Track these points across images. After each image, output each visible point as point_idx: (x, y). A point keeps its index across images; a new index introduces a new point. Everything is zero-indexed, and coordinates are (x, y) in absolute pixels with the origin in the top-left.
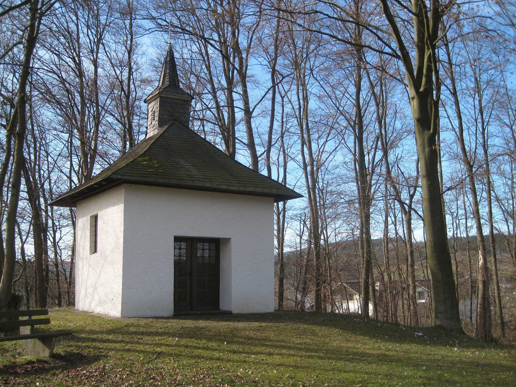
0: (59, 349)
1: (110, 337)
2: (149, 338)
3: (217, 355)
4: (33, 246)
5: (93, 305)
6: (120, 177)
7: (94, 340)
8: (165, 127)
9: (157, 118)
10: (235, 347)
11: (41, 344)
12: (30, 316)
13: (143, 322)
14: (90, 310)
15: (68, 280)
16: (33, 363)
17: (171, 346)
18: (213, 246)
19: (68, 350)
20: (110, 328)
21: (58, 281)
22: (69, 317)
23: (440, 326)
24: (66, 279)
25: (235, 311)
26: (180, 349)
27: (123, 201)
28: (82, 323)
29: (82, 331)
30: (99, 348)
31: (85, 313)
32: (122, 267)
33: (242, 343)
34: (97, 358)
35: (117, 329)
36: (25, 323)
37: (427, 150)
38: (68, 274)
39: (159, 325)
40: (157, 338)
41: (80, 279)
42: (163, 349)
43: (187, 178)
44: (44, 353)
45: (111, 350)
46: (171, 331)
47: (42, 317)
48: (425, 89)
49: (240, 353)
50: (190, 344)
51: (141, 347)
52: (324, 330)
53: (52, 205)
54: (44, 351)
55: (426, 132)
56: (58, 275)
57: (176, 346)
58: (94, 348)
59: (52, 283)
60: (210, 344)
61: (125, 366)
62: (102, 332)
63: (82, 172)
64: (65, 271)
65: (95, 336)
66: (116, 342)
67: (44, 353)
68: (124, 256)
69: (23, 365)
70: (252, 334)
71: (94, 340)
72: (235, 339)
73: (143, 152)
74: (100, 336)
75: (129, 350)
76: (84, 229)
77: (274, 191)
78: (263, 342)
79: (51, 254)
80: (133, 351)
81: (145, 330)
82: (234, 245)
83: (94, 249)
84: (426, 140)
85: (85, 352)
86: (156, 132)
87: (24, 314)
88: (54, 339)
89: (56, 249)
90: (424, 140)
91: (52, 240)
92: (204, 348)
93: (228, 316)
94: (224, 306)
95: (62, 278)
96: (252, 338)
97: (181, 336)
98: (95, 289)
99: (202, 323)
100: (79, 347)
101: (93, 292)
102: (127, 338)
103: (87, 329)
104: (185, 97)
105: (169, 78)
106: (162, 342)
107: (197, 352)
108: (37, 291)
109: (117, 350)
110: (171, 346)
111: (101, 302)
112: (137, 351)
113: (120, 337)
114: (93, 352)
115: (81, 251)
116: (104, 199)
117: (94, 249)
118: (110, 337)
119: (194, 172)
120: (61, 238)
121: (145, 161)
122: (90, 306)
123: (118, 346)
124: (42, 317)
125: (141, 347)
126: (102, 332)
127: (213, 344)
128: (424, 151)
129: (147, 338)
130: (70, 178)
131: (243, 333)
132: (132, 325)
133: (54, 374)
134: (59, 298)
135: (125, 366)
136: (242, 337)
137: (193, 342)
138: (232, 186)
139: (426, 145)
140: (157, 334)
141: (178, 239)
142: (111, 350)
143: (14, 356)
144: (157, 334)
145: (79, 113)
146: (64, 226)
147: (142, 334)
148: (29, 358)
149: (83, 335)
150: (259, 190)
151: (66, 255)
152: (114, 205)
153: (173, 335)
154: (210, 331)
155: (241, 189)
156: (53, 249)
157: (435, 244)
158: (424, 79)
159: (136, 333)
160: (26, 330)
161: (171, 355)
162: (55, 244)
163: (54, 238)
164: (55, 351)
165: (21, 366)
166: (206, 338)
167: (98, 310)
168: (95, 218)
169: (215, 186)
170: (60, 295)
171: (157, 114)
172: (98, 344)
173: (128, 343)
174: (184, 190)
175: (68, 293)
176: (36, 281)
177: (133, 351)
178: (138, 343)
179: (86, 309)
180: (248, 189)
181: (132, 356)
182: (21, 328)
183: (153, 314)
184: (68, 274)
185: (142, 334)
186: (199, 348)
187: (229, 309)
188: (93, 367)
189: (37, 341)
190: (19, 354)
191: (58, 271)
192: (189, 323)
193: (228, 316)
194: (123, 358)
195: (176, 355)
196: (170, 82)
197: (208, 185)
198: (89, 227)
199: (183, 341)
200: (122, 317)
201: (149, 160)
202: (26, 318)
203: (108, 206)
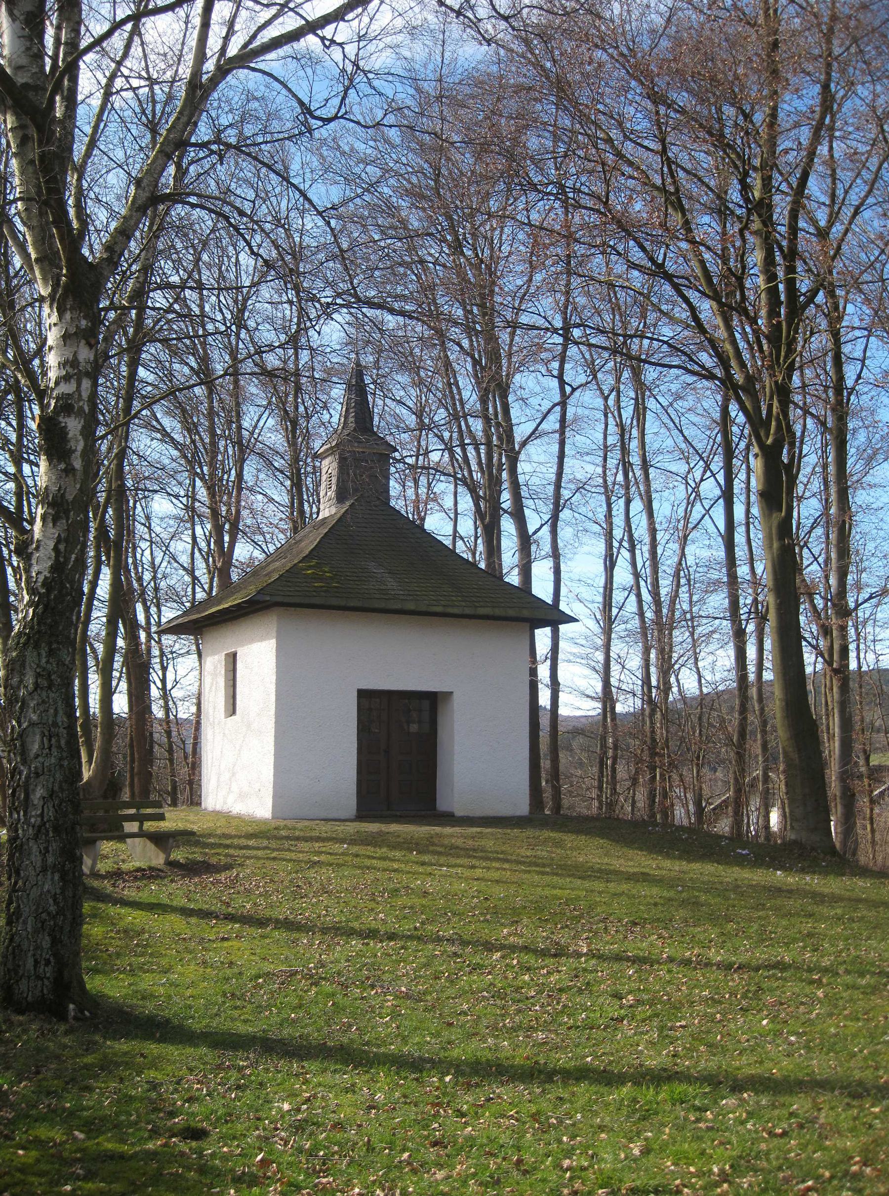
0: (179, 855)
1: (251, 843)
2: (306, 844)
3: (396, 866)
4: (126, 697)
5: (230, 800)
6: (268, 598)
7: (227, 847)
8: (348, 504)
9: (334, 487)
10: (426, 858)
11: (153, 846)
12: (138, 809)
13: (300, 825)
14: (225, 809)
15: (190, 760)
16: (144, 870)
17: (336, 854)
18: (426, 704)
19: (190, 857)
20: (252, 831)
21: (171, 760)
22: (192, 818)
23: (795, 842)
24: (186, 758)
25: (459, 813)
26: (346, 858)
27: (274, 634)
28: (211, 824)
29: (210, 835)
30: (232, 856)
31: (217, 813)
32: (273, 739)
33: (440, 854)
34: (228, 867)
35: (261, 832)
36: (131, 818)
37: (776, 545)
38: (189, 749)
39: (324, 829)
40: (317, 845)
41: (210, 757)
42: (323, 858)
43: (377, 596)
44: (158, 859)
45: (248, 858)
46: (341, 836)
47: (157, 811)
48: (775, 440)
49: (432, 865)
50: (361, 852)
51: (293, 856)
52: (569, 839)
53: (160, 633)
54: (157, 856)
55: (774, 515)
56: (170, 751)
57: (343, 854)
58: (226, 855)
59: (159, 765)
60: (391, 854)
61: (265, 876)
62: (240, 837)
63: (214, 561)
64: (184, 742)
65: (228, 842)
66: (258, 849)
67: (158, 859)
68: (276, 722)
69: (131, 872)
70: (459, 842)
71: (227, 847)
72: (431, 848)
73: (307, 552)
74: (236, 841)
75: (274, 859)
76: (215, 675)
77: (526, 613)
78: (468, 852)
79: (158, 712)
80: (280, 859)
81: (302, 834)
82: (457, 701)
83: (232, 709)
84: (774, 531)
85: (214, 860)
86: (334, 510)
87: (128, 805)
88: (171, 840)
89: (166, 703)
90: (770, 528)
91: (160, 685)
92: (380, 858)
93: (449, 819)
94: (442, 805)
95: (178, 755)
96: (457, 847)
97: (352, 842)
98: (234, 774)
99: (394, 827)
100: (206, 854)
101: (230, 780)
102: (274, 844)
103: (219, 832)
104: (383, 450)
105: (355, 417)
106: (324, 849)
107: (368, 862)
108: (136, 780)
109: (258, 858)
110: (336, 854)
111: (242, 796)
112: (284, 860)
113: (265, 843)
114: (224, 860)
115: (211, 711)
116: (245, 628)
117: (232, 709)
118: (251, 843)
119: (391, 584)
120: (176, 682)
121: (310, 567)
122: (225, 803)
123: (260, 853)
124: (157, 811)
125: (293, 856)
126: (240, 837)
127: (398, 854)
128: (771, 547)
129: (303, 845)
130: (191, 572)
131: (446, 842)
132: (286, 827)
133: (172, 881)
134: (174, 794)
135: (265, 876)
136: (442, 846)
137: (369, 850)
138: (452, 606)
139: (774, 537)
140: (318, 839)
141: (362, 694)
142: (248, 858)
143: (116, 863)
144: (318, 839)
145: (207, 453)
146: (182, 655)
147: (298, 839)
148: (138, 864)
149: (212, 840)
150: (498, 612)
151: (185, 711)
152: (262, 639)
153: (343, 841)
154: (399, 836)
155: (468, 611)
156: (161, 702)
157: (787, 704)
158: (773, 423)
159: (288, 838)
160: (131, 827)
161: (331, 865)
162: (165, 694)
163: (164, 681)
164: (172, 857)
165: (129, 873)
166: (388, 846)
167: (238, 808)
168: (233, 658)
169: (424, 608)
170: (174, 788)
171: (334, 480)
172: (231, 851)
173: (274, 850)
174: (374, 614)
175: (191, 783)
176: (133, 761)
177: (280, 859)
178: (289, 850)
179: (218, 808)
180: (482, 611)
181: (275, 865)
182: (126, 824)
183: (324, 815)
184: (189, 749)
185: (298, 839)
186: (374, 858)
187: (449, 810)
188: (222, 877)
189: (148, 843)
190: (123, 861)
191: (170, 744)
192: (373, 827)
193: (449, 819)
194: (264, 867)
195: (337, 865)
196: (356, 422)
197: (411, 606)
198: (223, 672)
199: (355, 849)
200: (273, 818)
201: (318, 566)
202: (132, 811)
203: (252, 641)
